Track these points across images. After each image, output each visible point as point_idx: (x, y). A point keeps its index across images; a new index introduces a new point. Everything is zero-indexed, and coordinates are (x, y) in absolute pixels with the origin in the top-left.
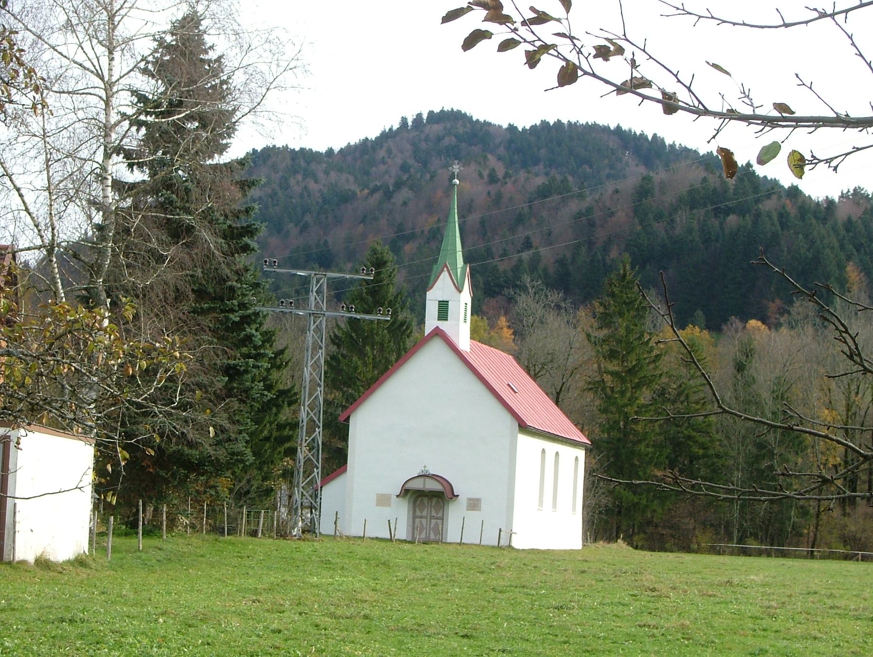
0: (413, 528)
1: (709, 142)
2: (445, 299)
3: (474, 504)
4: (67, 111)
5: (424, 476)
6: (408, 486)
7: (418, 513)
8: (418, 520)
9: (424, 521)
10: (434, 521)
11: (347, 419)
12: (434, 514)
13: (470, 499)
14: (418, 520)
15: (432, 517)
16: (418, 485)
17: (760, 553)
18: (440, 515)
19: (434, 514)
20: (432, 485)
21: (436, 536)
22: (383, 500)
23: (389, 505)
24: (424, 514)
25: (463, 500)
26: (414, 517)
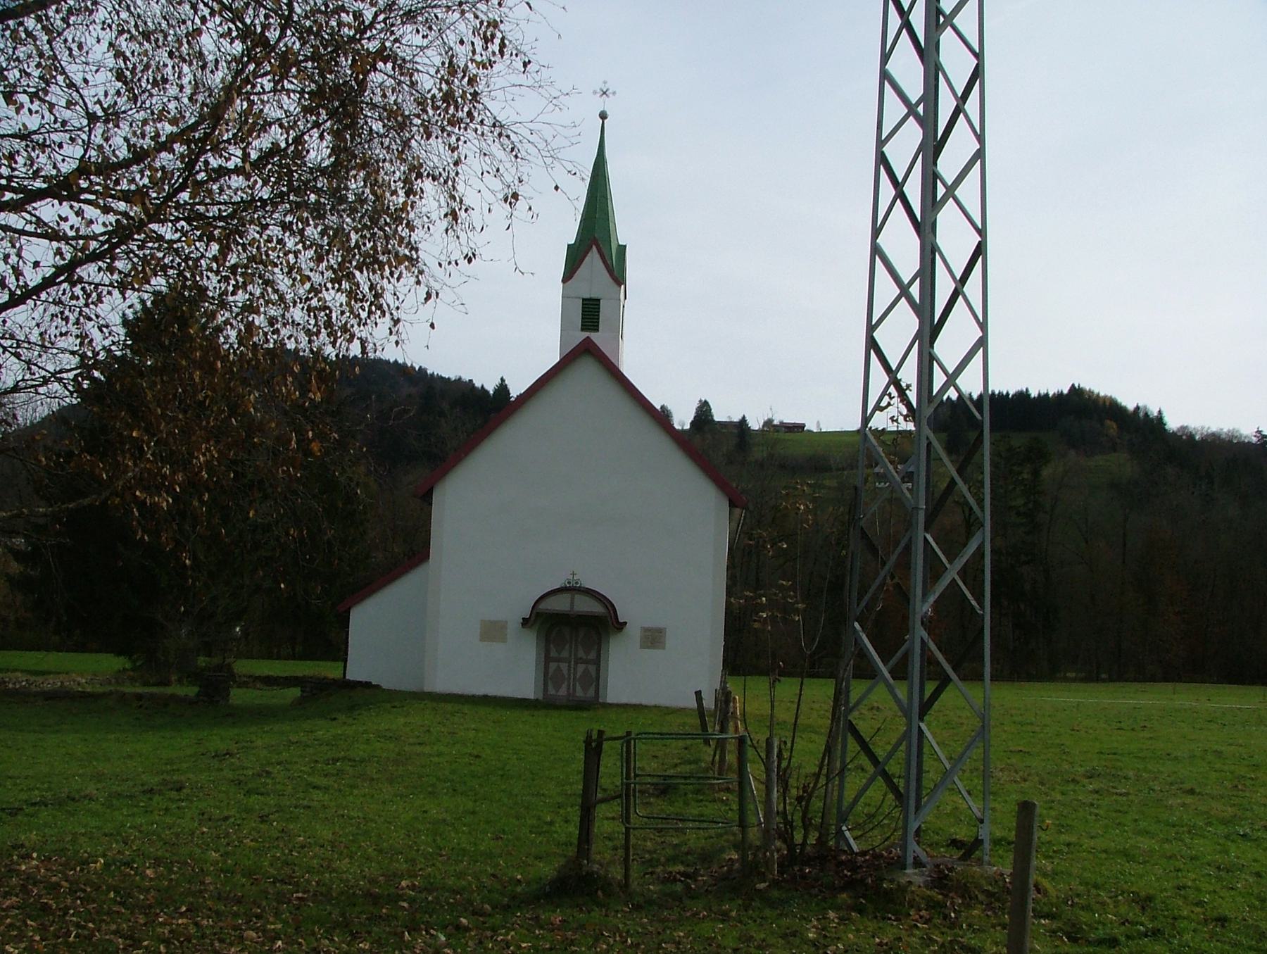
0: (547, 676)
1: (603, 116)
2: (593, 296)
3: (654, 638)
4: (73, 243)
5: (571, 589)
6: (542, 606)
7: (553, 654)
8: (553, 666)
9: (564, 666)
10: (581, 668)
11: (427, 497)
12: (581, 654)
13: (646, 630)
14: (553, 666)
15: (578, 661)
16: (560, 604)
17: (1074, 680)
18: (592, 655)
19: (581, 654)
20: (585, 606)
21: (559, 668)
22: (492, 631)
23: (504, 640)
24: (565, 654)
25: (633, 631)
26: (548, 659)
